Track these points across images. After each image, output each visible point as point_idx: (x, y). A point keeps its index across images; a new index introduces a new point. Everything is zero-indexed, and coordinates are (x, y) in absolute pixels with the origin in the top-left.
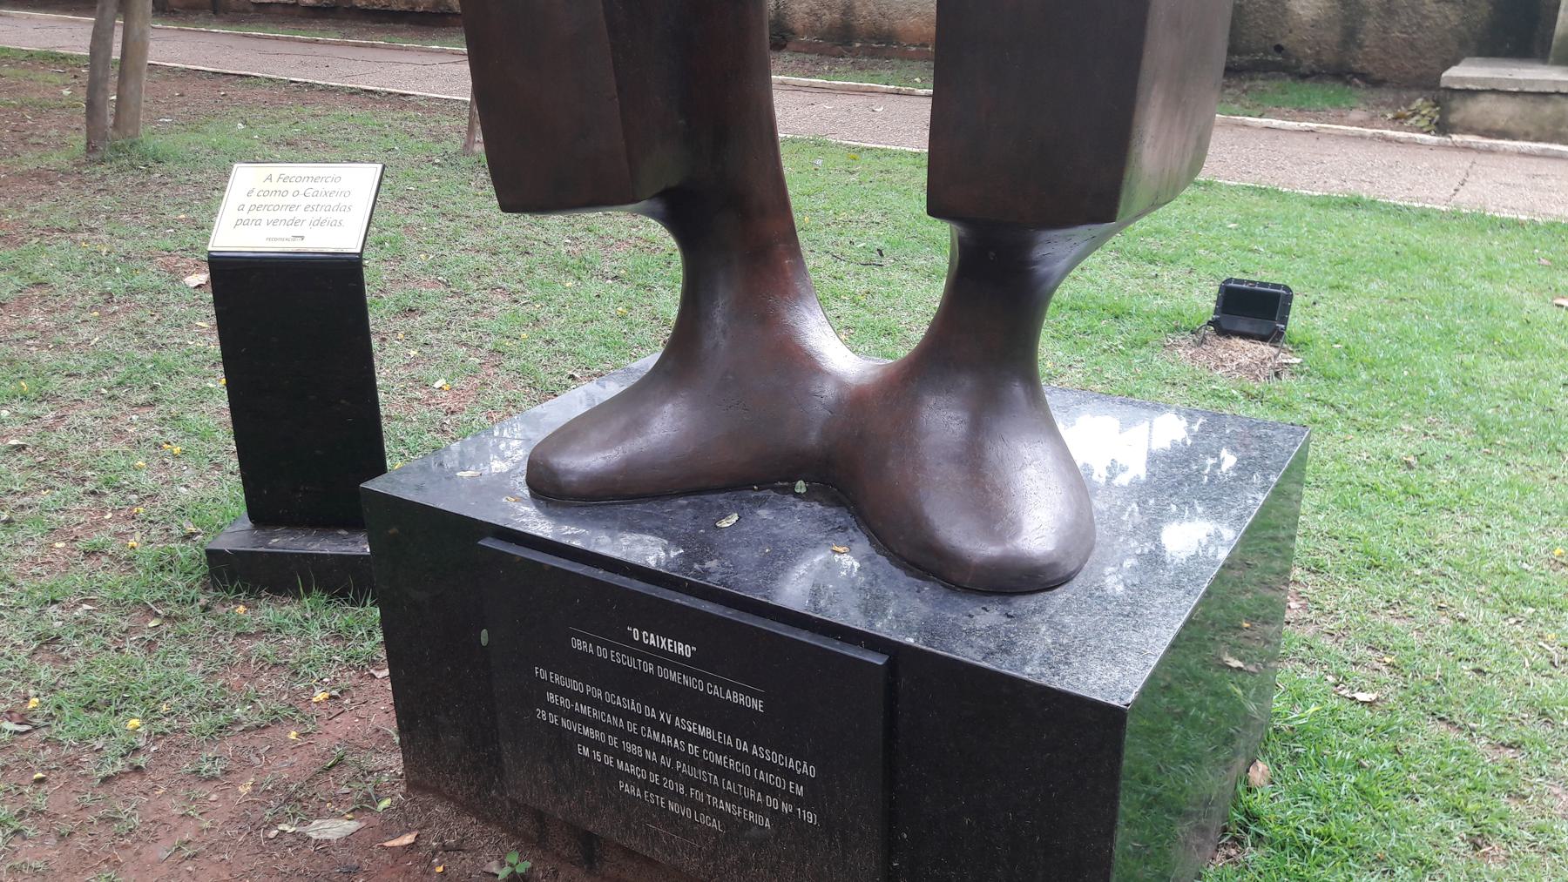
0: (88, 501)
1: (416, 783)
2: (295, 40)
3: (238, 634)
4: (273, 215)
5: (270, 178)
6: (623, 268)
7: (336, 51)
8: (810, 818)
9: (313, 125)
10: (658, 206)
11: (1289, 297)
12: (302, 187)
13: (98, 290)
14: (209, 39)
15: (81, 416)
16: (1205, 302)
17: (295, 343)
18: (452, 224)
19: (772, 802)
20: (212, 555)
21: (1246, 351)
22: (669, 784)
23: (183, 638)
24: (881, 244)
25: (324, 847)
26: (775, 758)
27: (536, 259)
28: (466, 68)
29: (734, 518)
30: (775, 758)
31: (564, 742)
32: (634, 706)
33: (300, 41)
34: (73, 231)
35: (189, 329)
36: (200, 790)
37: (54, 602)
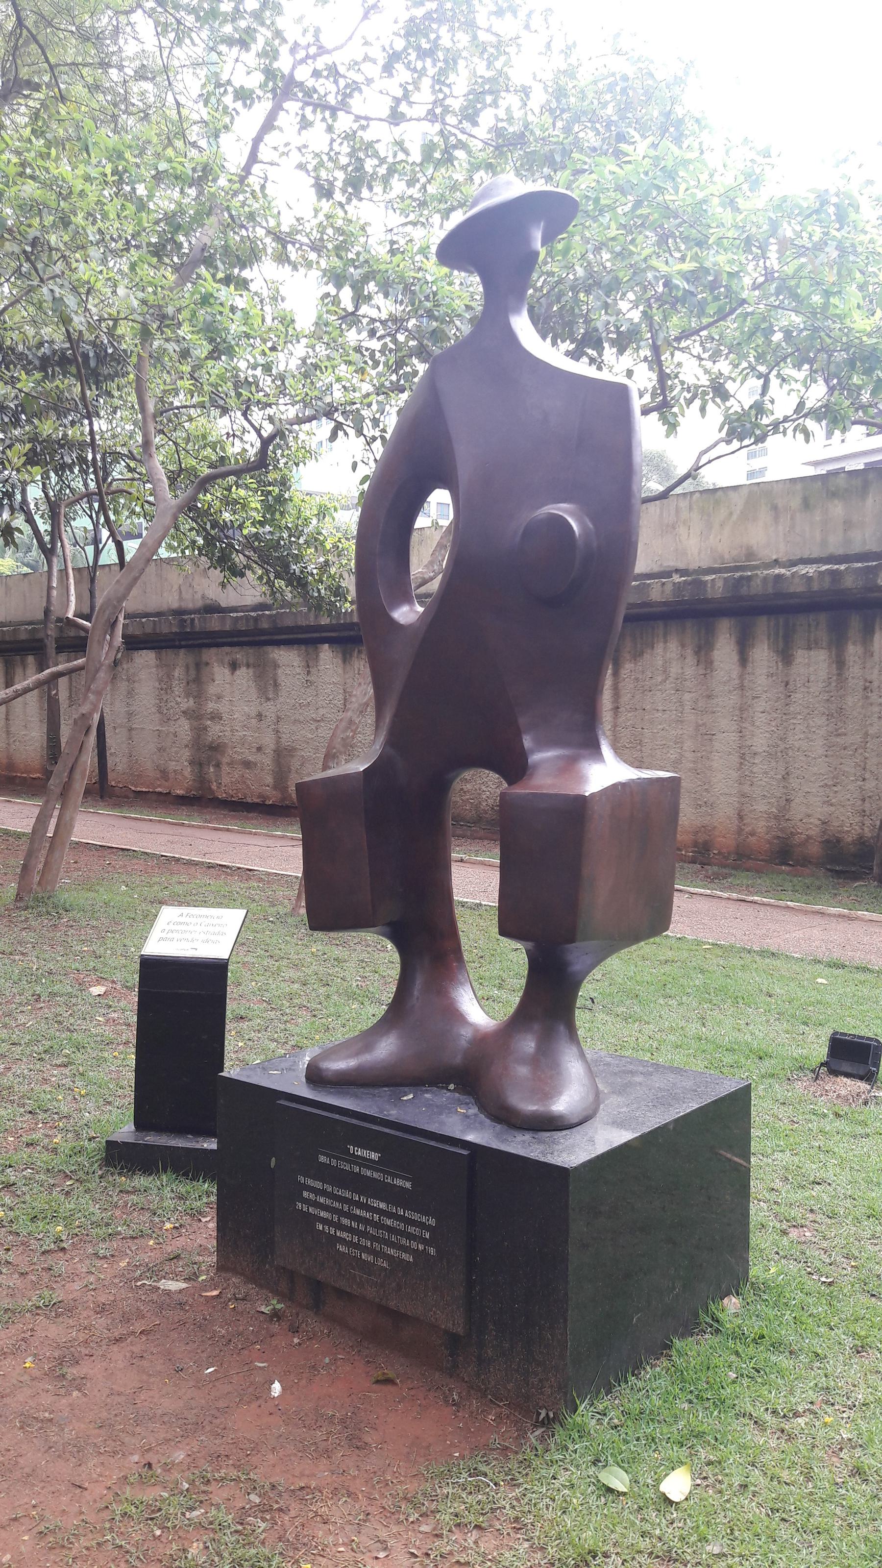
0: (28, 1116)
1: (222, 1267)
2: (165, 822)
3: (121, 1191)
4: (180, 936)
5: (182, 915)
6: (370, 963)
7: (198, 833)
8: (432, 1251)
9: (179, 889)
10: (387, 929)
11: (835, 1033)
12: (199, 920)
13: (31, 993)
14: (96, 818)
15: (22, 1068)
16: (821, 1052)
17: (182, 1006)
18: (277, 964)
19: (414, 1245)
20: (111, 1145)
21: (847, 1086)
22: (363, 1242)
23: (87, 1191)
24: (593, 995)
25: (168, 1293)
26: (416, 1216)
27: (333, 989)
28: (300, 850)
29: (411, 1096)
30: (416, 1216)
31: (310, 1220)
32: (348, 1194)
33: (169, 823)
34: (11, 954)
35: (91, 1021)
36: (99, 1263)
37: (10, 1166)
